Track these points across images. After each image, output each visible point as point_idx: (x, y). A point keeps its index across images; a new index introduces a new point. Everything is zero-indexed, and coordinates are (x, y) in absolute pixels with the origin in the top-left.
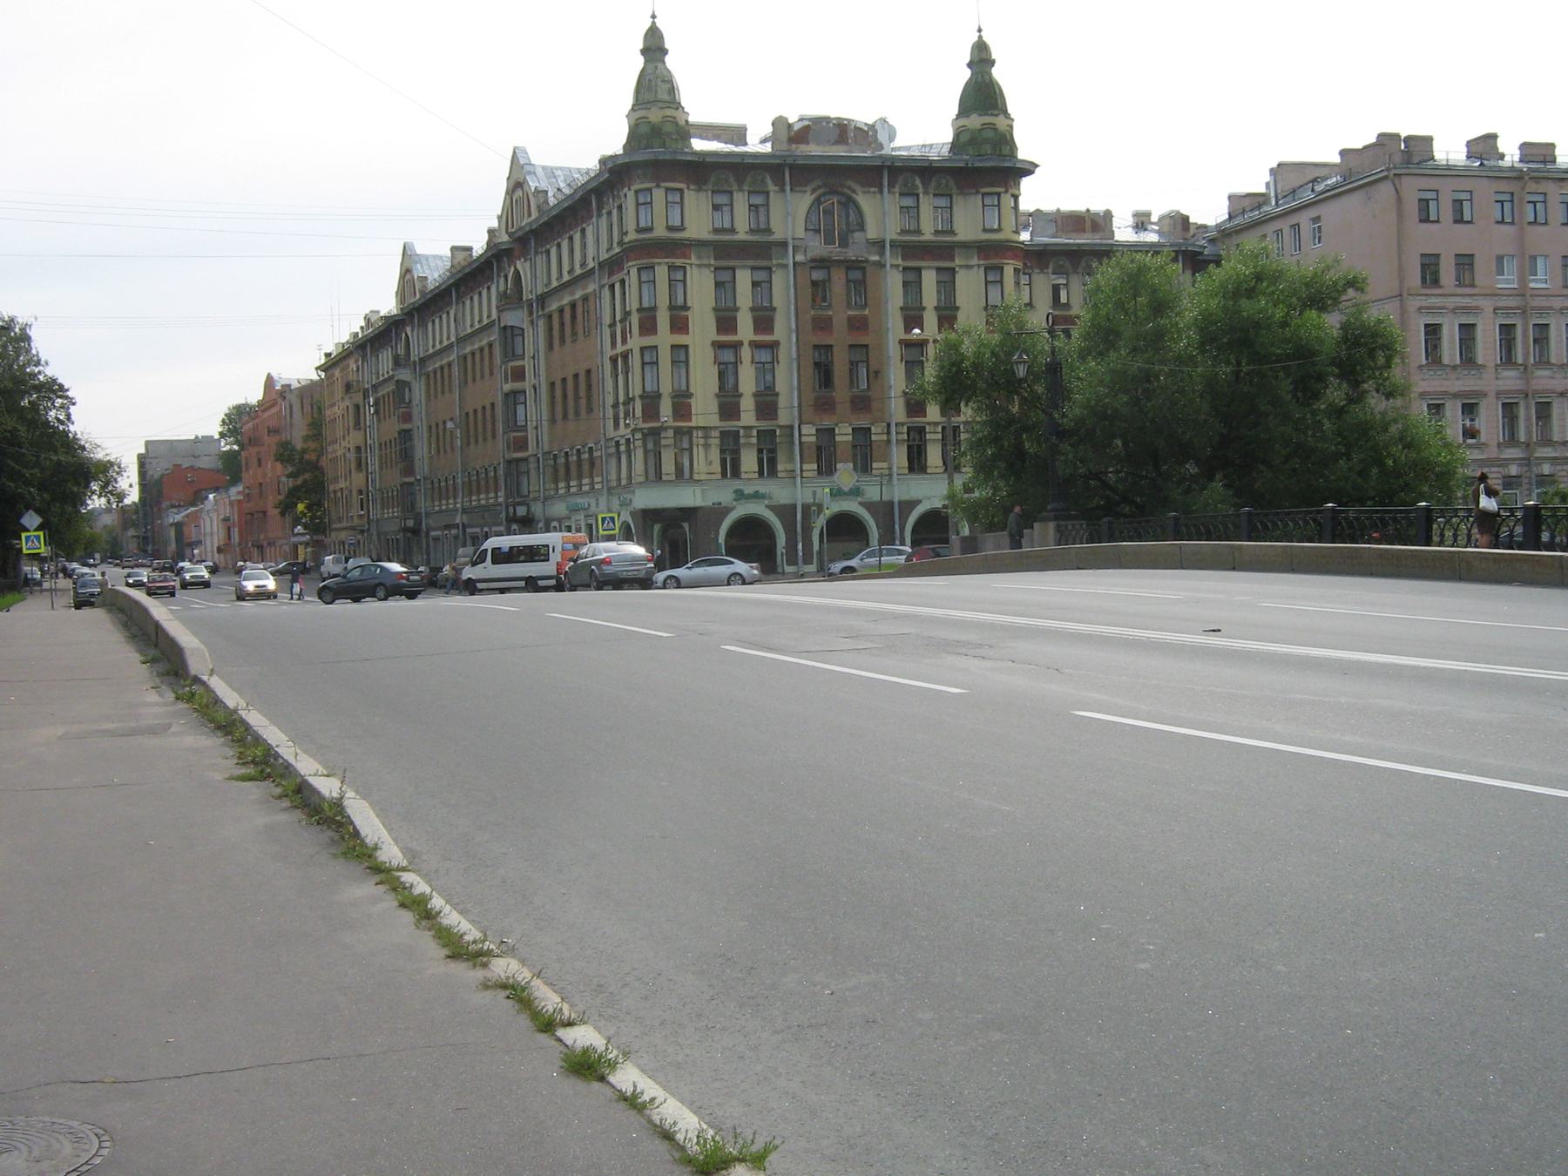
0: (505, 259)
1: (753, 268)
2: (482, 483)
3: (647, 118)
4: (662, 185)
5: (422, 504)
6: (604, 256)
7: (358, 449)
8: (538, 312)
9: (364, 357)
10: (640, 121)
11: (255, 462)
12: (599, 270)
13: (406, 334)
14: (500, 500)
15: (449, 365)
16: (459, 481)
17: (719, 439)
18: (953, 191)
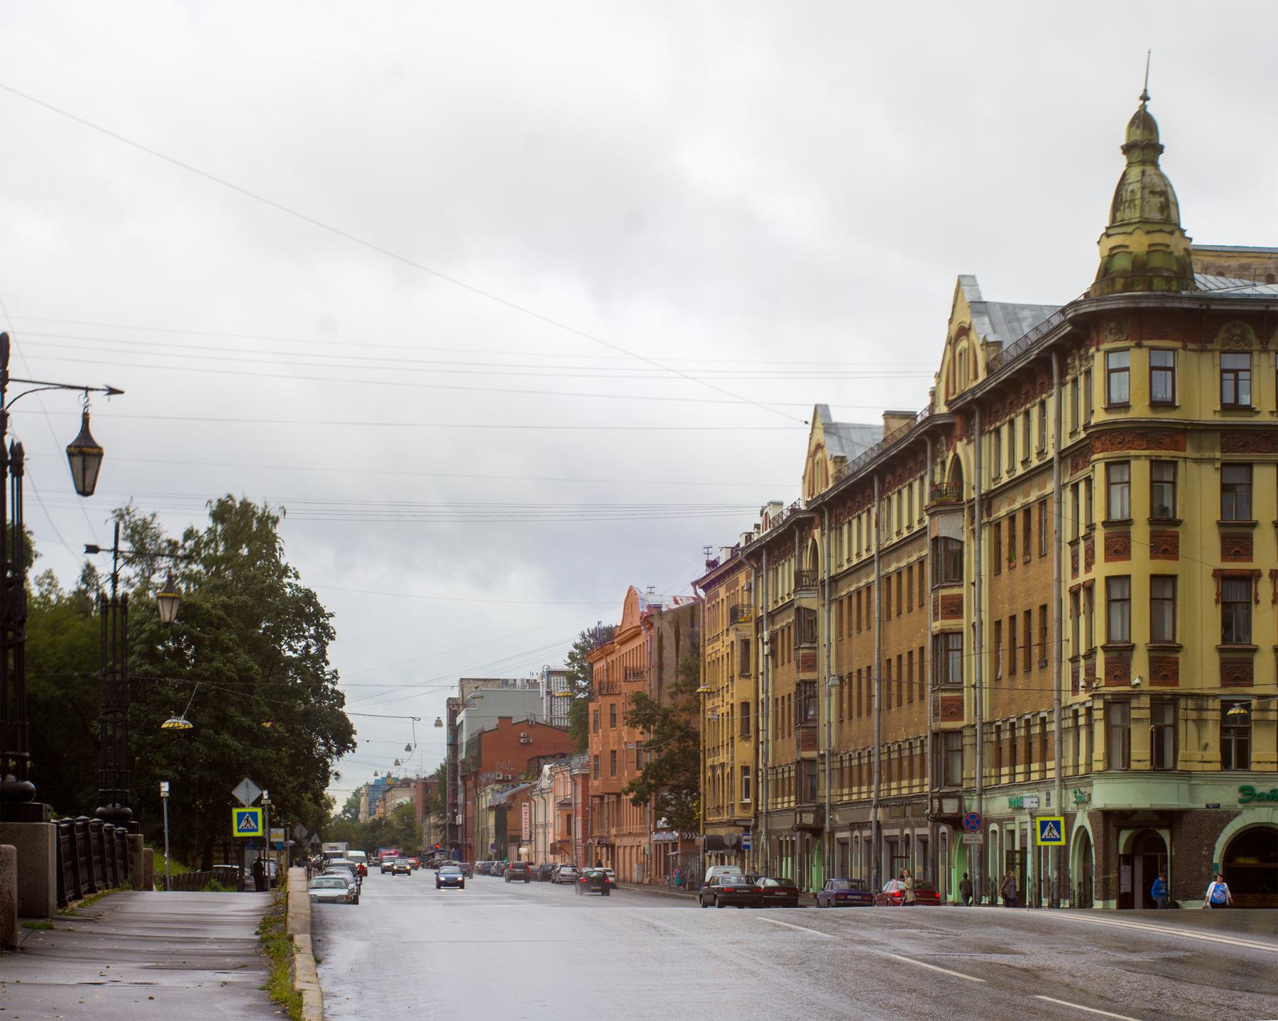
0: (943, 438)
1: (730, 883)
2: (905, 763)
3: (1127, 247)
4: (1145, 343)
5: (827, 791)
6: (1067, 442)
7: (745, 705)
8: (981, 518)
9: (758, 571)
10: (1115, 251)
11: (606, 719)
12: (1060, 463)
13: (814, 540)
14: (1050, 775)
15: (869, 588)
16: (875, 759)
17: (1149, 711)
18: (1254, 347)
